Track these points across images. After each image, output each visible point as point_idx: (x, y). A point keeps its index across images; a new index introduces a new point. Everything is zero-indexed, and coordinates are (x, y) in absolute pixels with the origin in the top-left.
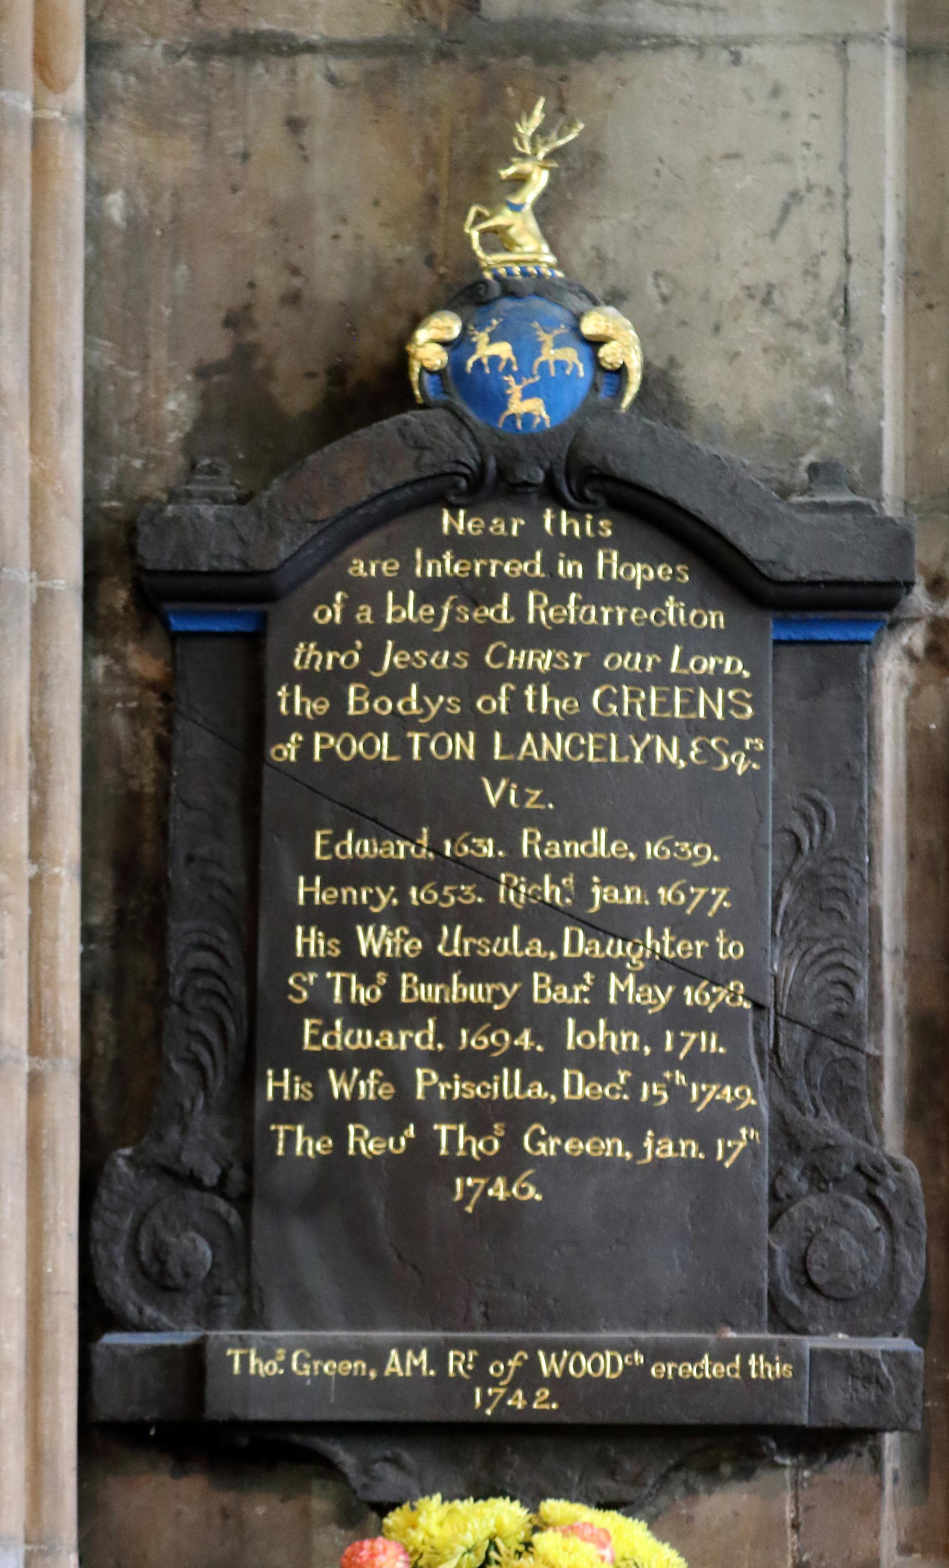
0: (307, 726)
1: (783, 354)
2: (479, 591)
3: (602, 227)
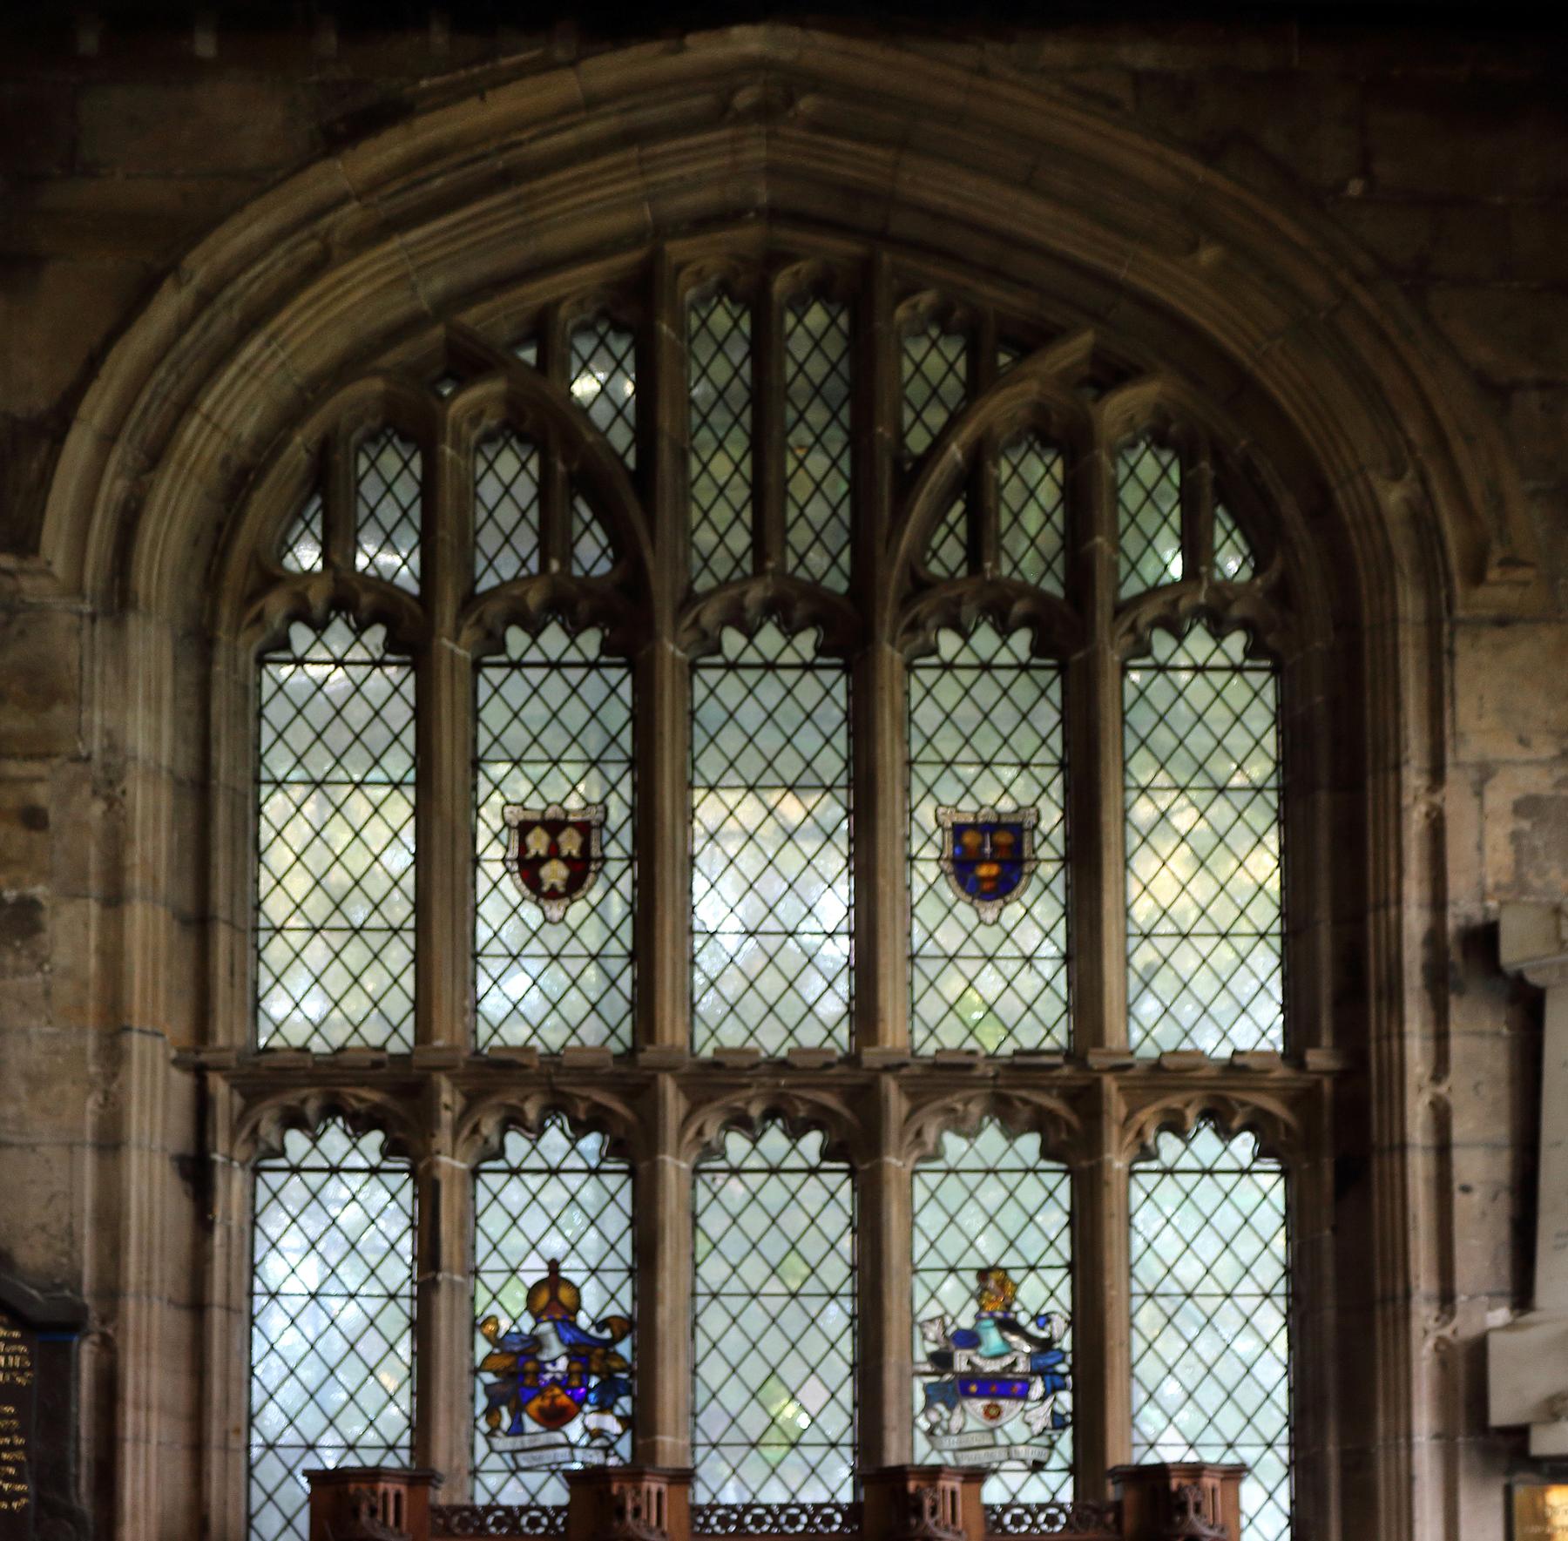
1: (48, 1246)
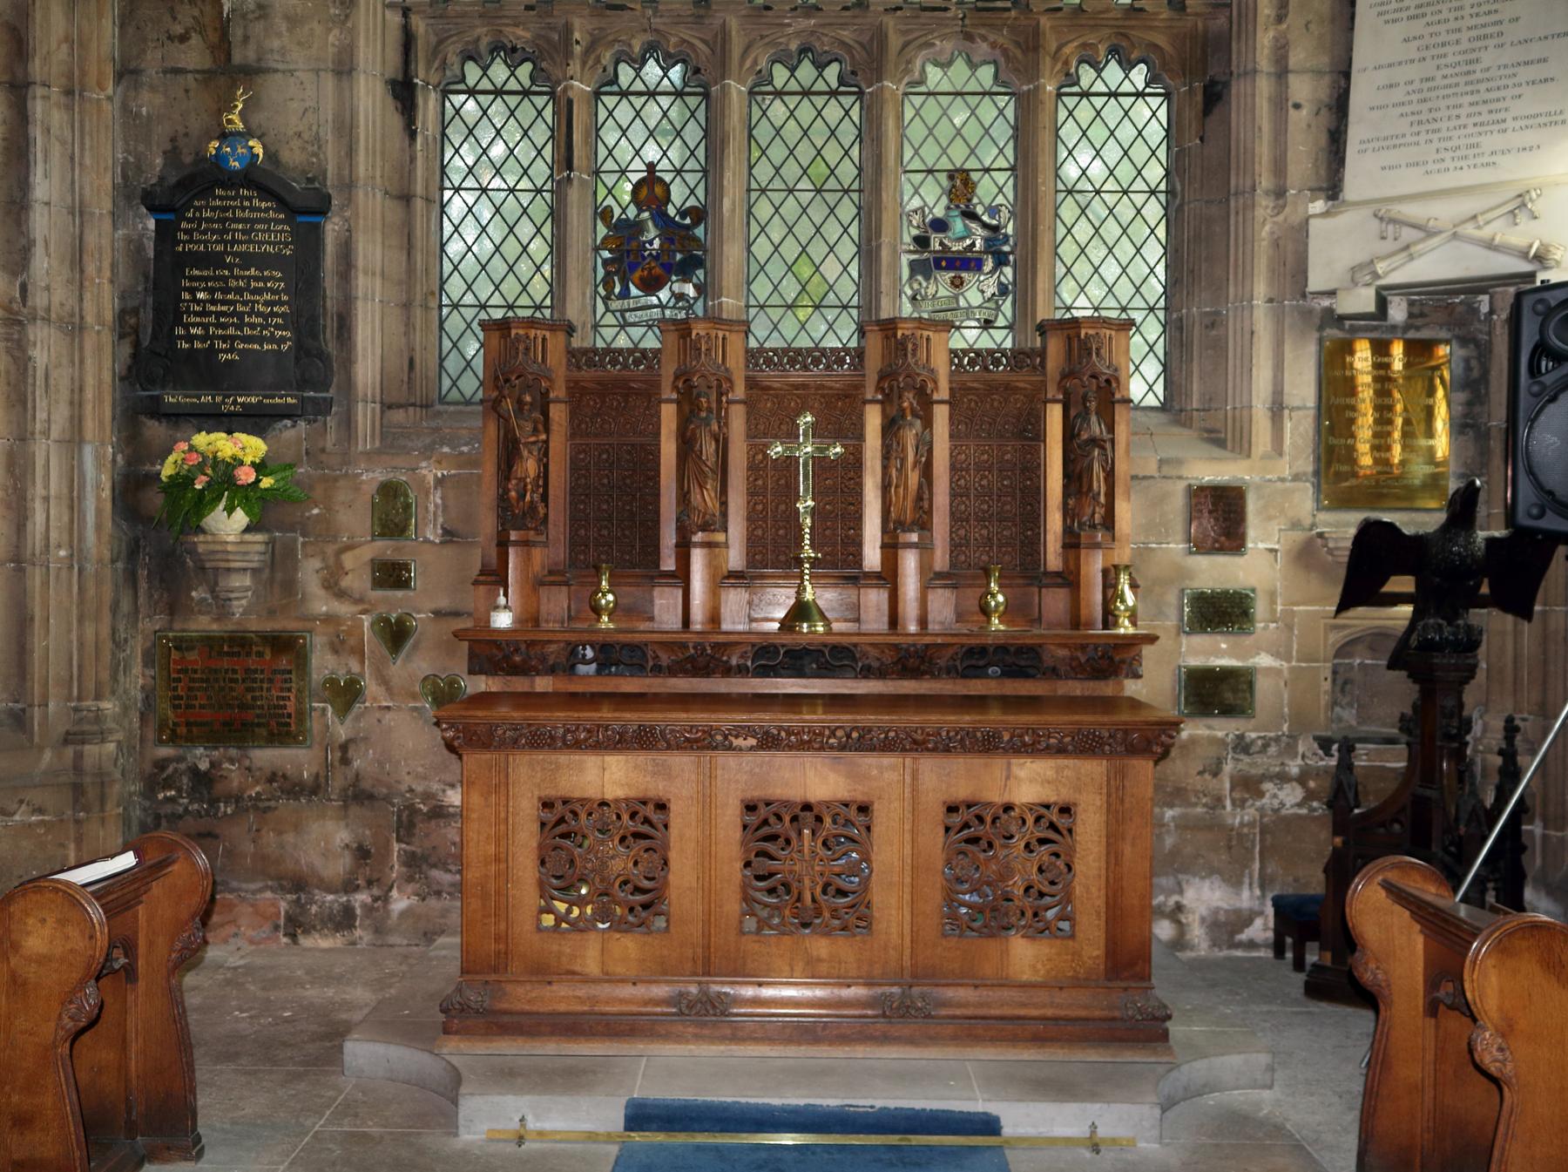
0: (184, 242)
1: (304, 149)
2: (225, 209)
3: (258, 118)
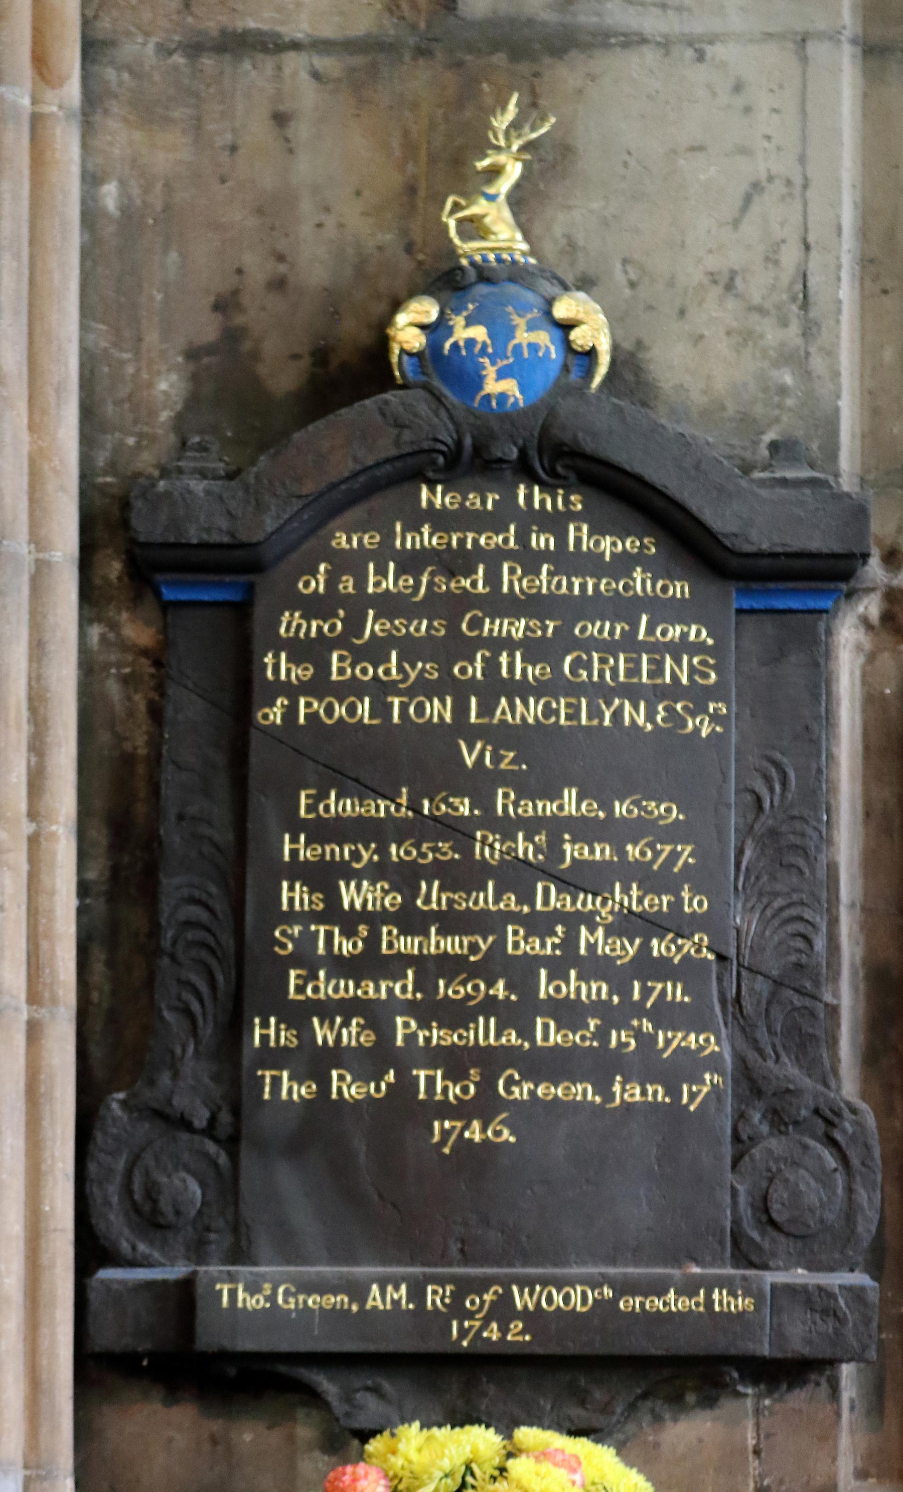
1: (745, 337)
